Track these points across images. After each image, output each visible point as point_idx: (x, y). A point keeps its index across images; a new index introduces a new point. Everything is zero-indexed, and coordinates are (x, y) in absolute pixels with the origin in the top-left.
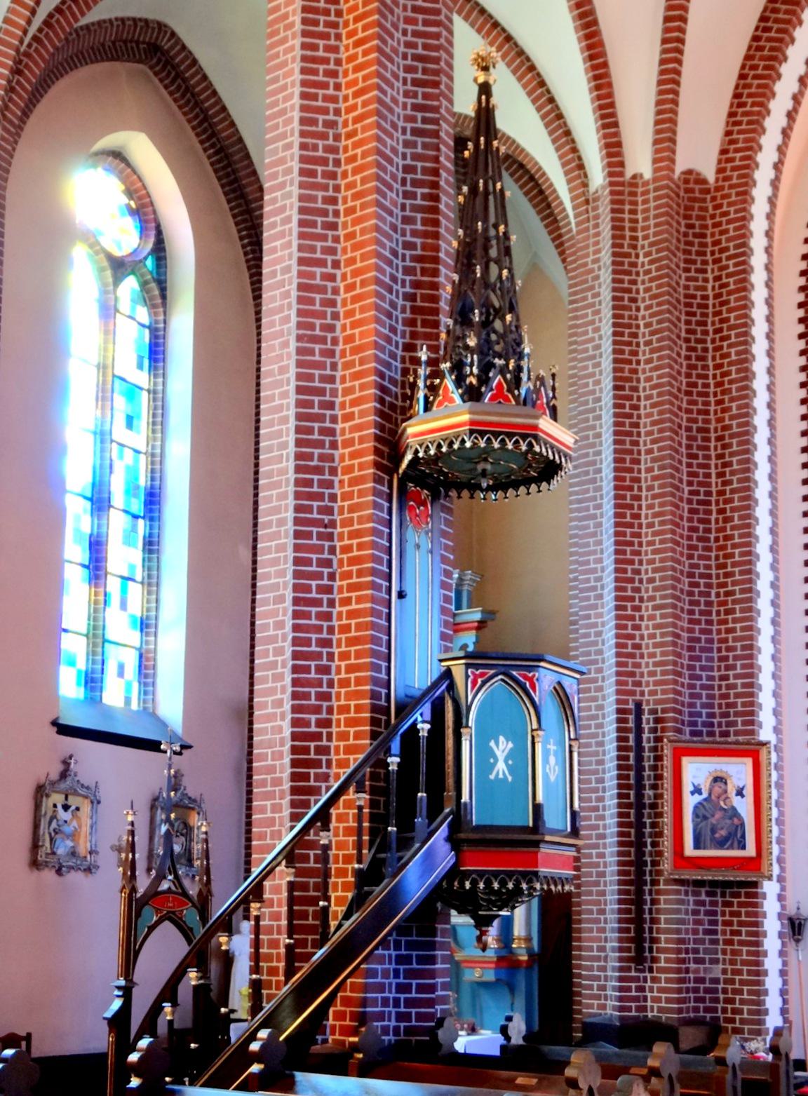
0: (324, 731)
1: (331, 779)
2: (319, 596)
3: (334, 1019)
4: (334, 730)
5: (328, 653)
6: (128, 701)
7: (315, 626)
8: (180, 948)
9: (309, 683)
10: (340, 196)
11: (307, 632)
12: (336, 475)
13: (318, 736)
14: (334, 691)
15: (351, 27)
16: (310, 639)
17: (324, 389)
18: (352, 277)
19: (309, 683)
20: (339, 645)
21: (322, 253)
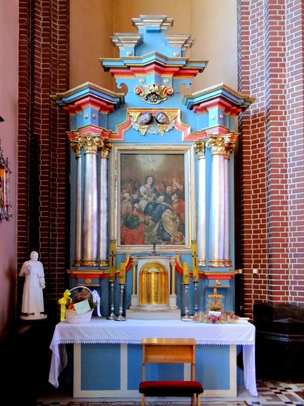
0: (284, 132)
1: (286, 87)
2: (280, 15)
3: (290, 231)
4: (289, 227)
5: (287, 270)
6: (26, 315)
7: (279, 144)
8: (190, 364)
9: (276, 39)
10: (286, 53)
11: (277, 209)
12: (288, 210)
13: (281, 134)
14: (286, 116)
15: (290, 13)
16: (277, 96)
17: (281, 193)
18: (292, 97)
19: (276, 39)
20: (290, 193)
21: (280, 66)
